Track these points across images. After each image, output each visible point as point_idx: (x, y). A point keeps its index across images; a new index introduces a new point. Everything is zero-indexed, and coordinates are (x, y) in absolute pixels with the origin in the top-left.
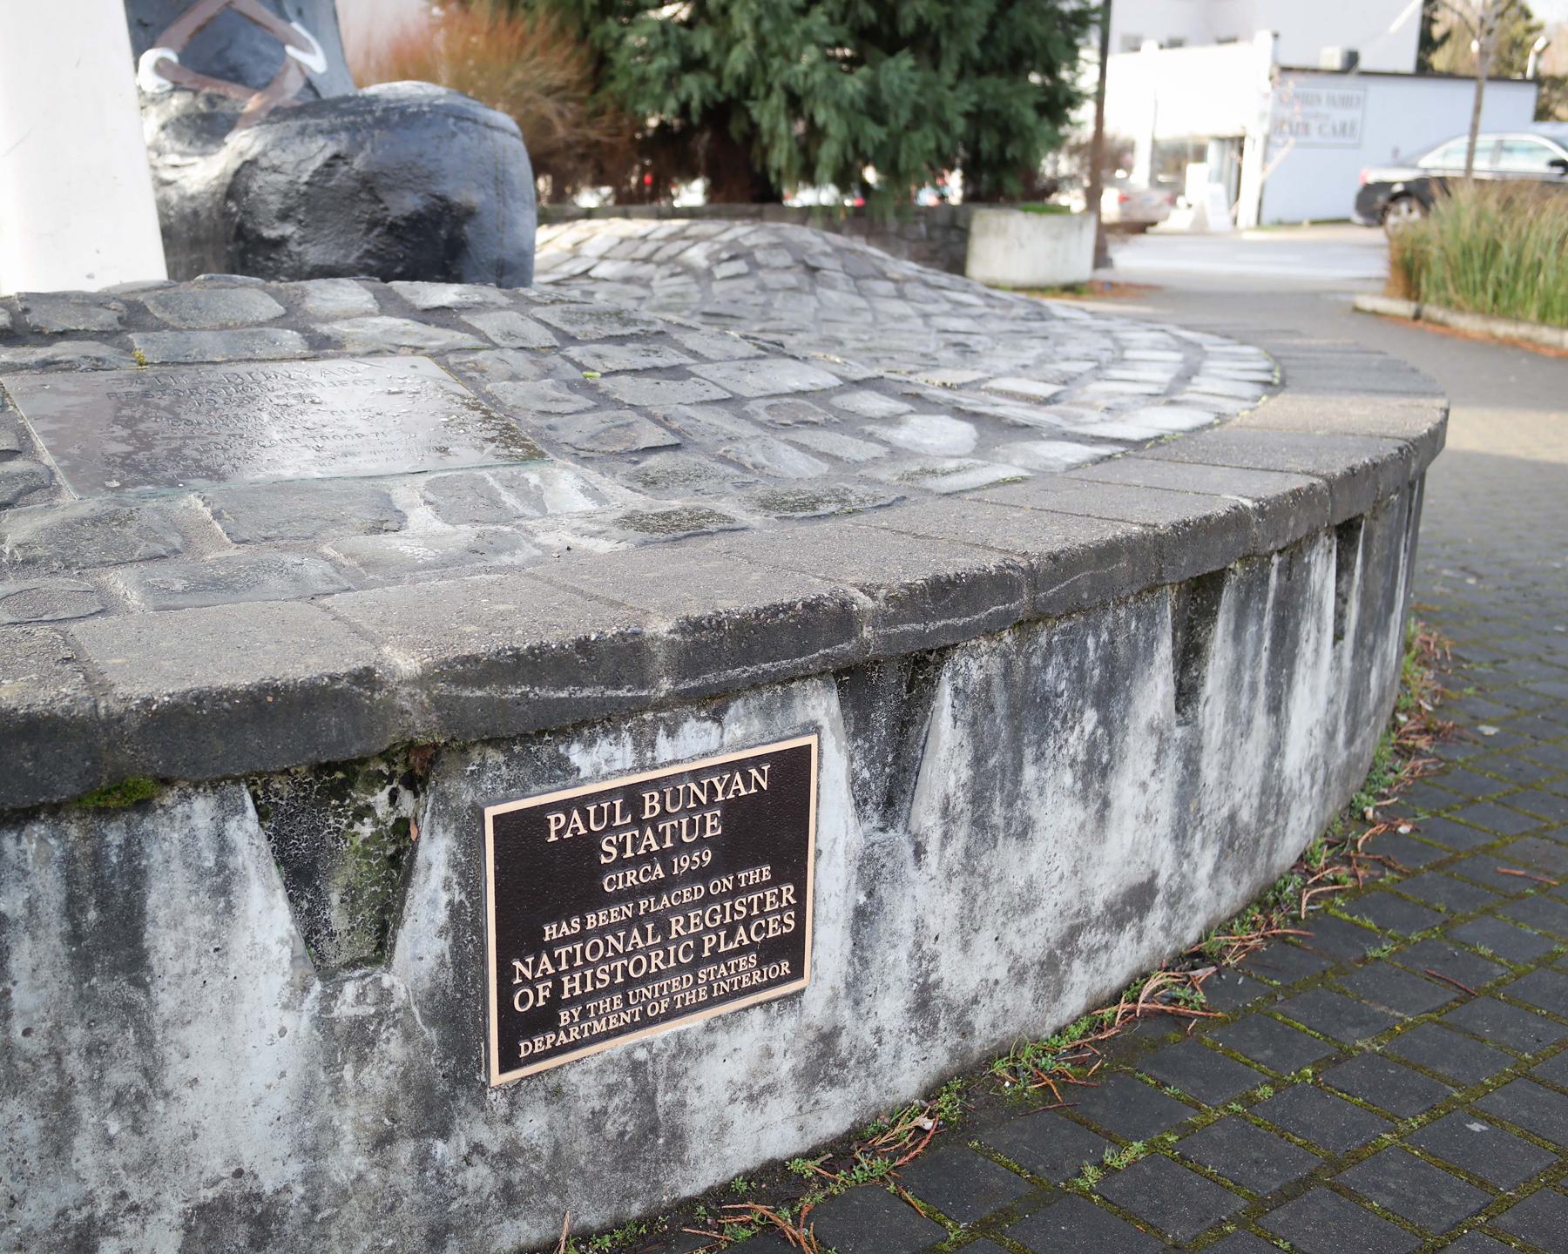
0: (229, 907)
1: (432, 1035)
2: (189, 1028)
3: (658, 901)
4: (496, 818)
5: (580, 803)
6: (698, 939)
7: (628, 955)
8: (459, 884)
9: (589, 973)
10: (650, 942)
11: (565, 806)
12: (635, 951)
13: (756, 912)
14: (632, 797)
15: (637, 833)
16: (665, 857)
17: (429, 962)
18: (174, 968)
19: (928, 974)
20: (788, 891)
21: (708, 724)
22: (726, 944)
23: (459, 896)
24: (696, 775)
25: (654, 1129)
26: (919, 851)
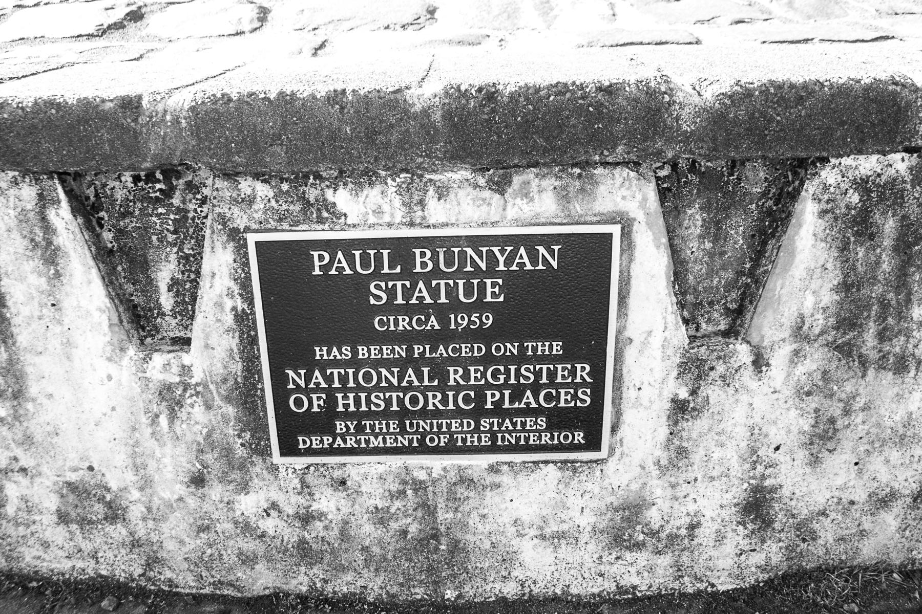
0: (58, 275)
1: (230, 410)
2: (41, 357)
3: (434, 349)
4: (258, 244)
5: (347, 246)
6: (480, 392)
7: (405, 390)
8: (241, 295)
9: (363, 396)
10: (426, 383)
11: (330, 246)
12: (410, 387)
13: (544, 380)
14: (402, 249)
15: (408, 283)
16: (442, 313)
17: (220, 353)
18: (25, 311)
19: (763, 477)
20: (583, 371)
21: (487, 194)
22: (511, 402)
23: (240, 305)
24: (475, 242)
25: (436, 536)
26: (759, 363)
